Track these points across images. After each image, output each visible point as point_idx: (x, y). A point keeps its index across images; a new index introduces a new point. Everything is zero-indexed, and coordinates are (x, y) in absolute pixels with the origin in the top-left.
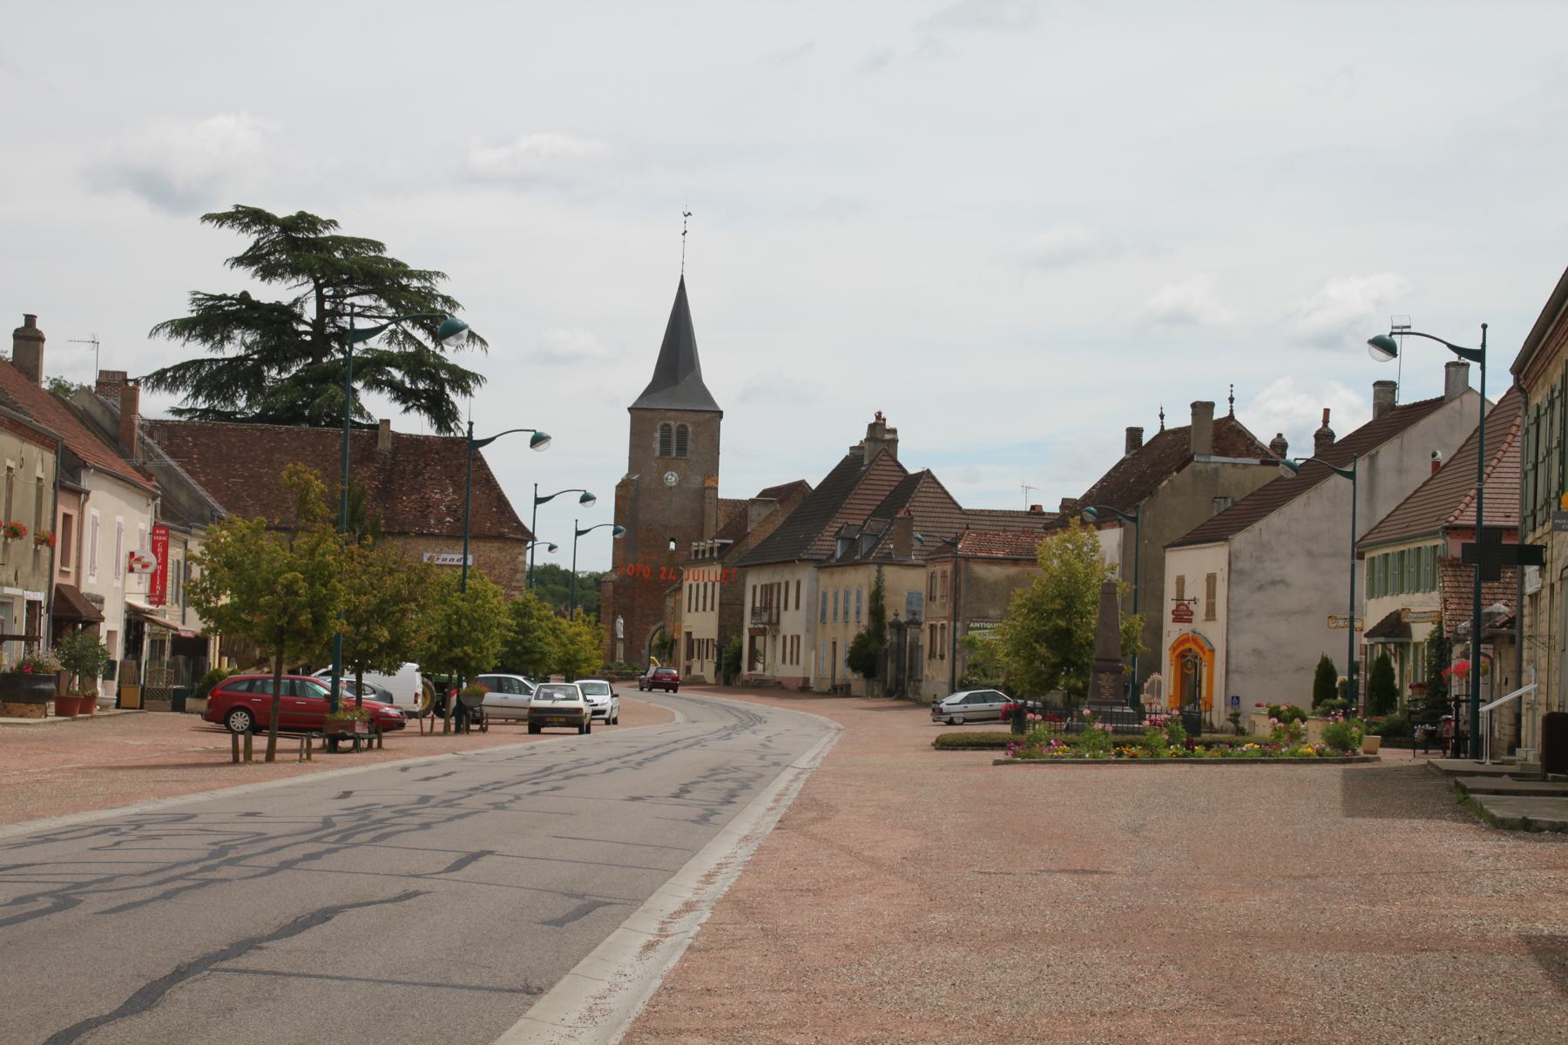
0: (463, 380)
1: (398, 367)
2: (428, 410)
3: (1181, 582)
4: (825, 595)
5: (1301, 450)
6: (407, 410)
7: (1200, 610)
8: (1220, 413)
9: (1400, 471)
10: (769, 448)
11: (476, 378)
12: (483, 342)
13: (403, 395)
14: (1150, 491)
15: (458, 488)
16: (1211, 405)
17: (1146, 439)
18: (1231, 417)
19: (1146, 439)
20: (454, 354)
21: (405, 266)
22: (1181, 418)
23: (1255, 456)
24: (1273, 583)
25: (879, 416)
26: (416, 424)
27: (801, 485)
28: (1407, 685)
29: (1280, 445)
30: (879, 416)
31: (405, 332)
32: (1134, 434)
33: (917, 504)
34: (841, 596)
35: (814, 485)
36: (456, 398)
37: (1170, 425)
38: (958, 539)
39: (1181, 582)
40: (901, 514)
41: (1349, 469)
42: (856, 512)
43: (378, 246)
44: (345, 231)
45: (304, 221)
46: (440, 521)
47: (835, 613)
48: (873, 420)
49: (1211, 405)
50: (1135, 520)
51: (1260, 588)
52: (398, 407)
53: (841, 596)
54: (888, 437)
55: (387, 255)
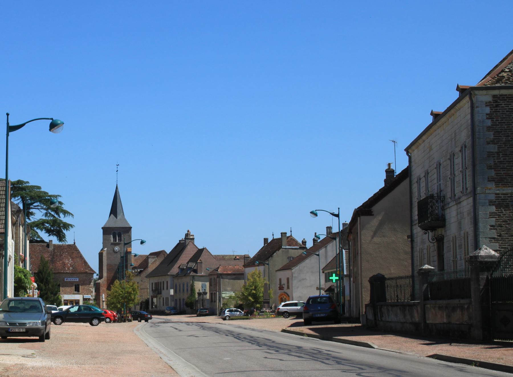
0: (67, 226)
1: (48, 223)
2: (57, 236)
3: (280, 280)
4: (176, 285)
5: (309, 245)
6: (49, 235)
7: (285, 287)
8: (288, 235)
9: (326, 257)
10: (151, 239)
11: (72, 226)
12: (72, 215)
13: (49, 231)
14: (271, 256)
15: (73, 258)
16: (286, 233)
17: (269, 241)
18: (291, 236)
19: (269, 241)
20: (63, 218)
21: (47, 193)
22: (278, 236)
23: (298, 246)
24: (303, 279)
25: (188, 231)
26: (55, 240)
27: (163, 252)
28: (79, 297)
29: (304, 243)
30: (188, 231)
31: (50, 213)
32: (266, 240)
33: (203, 257)
34: (185, 286)
35: (168, 252)
36: (65, 231)
37: (276, 237)
38: (218, 268)
39: (280, 280)
40: (199, 261)
41: (318, 253)
42: (184, 260)
43: (39, 188)
44: (32, 183)
45: (19, 182)
46: (69, 269)
47: (180, 290)
48: (187, 232)
49: (286, 233)
50: (268, 264)
51: (300, 281)
52: (47, 234)
53: (185, 286)
54: (191, 237)
55: (42, 190)
